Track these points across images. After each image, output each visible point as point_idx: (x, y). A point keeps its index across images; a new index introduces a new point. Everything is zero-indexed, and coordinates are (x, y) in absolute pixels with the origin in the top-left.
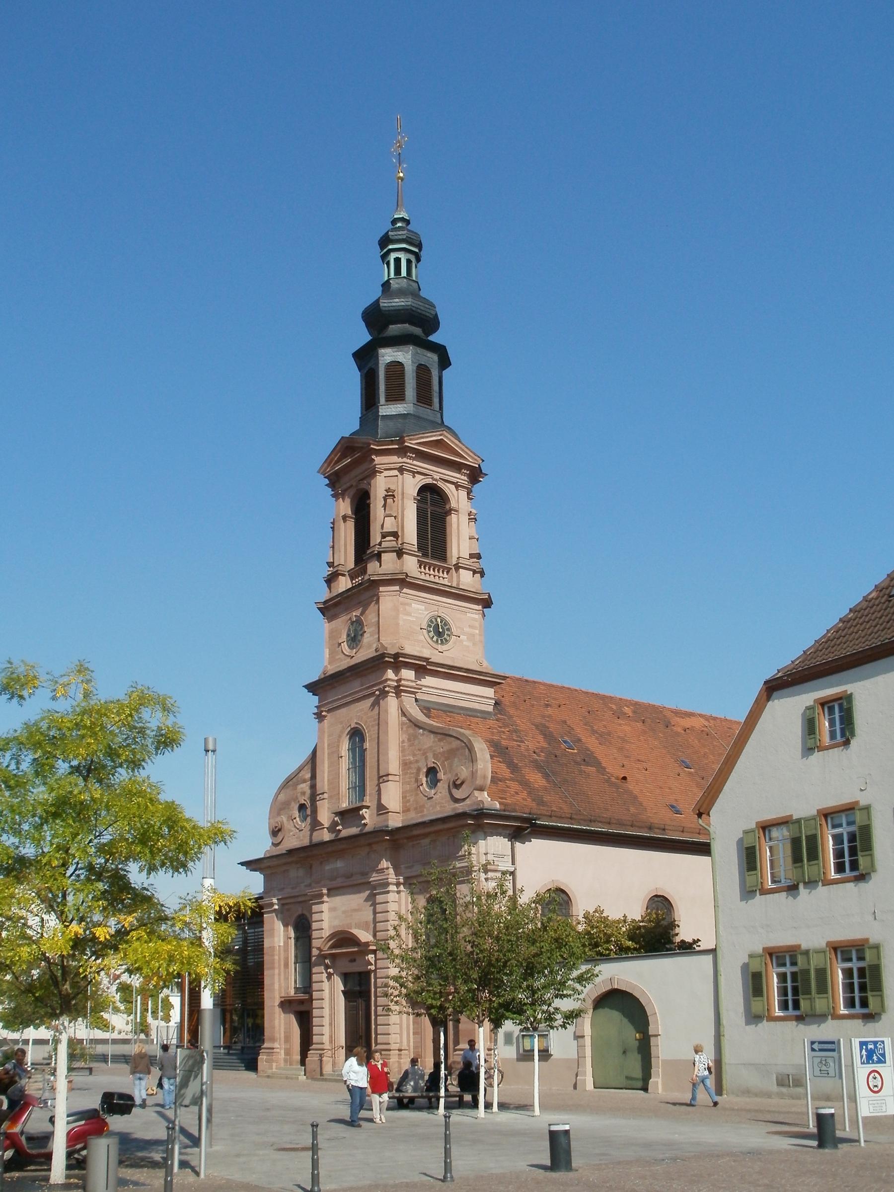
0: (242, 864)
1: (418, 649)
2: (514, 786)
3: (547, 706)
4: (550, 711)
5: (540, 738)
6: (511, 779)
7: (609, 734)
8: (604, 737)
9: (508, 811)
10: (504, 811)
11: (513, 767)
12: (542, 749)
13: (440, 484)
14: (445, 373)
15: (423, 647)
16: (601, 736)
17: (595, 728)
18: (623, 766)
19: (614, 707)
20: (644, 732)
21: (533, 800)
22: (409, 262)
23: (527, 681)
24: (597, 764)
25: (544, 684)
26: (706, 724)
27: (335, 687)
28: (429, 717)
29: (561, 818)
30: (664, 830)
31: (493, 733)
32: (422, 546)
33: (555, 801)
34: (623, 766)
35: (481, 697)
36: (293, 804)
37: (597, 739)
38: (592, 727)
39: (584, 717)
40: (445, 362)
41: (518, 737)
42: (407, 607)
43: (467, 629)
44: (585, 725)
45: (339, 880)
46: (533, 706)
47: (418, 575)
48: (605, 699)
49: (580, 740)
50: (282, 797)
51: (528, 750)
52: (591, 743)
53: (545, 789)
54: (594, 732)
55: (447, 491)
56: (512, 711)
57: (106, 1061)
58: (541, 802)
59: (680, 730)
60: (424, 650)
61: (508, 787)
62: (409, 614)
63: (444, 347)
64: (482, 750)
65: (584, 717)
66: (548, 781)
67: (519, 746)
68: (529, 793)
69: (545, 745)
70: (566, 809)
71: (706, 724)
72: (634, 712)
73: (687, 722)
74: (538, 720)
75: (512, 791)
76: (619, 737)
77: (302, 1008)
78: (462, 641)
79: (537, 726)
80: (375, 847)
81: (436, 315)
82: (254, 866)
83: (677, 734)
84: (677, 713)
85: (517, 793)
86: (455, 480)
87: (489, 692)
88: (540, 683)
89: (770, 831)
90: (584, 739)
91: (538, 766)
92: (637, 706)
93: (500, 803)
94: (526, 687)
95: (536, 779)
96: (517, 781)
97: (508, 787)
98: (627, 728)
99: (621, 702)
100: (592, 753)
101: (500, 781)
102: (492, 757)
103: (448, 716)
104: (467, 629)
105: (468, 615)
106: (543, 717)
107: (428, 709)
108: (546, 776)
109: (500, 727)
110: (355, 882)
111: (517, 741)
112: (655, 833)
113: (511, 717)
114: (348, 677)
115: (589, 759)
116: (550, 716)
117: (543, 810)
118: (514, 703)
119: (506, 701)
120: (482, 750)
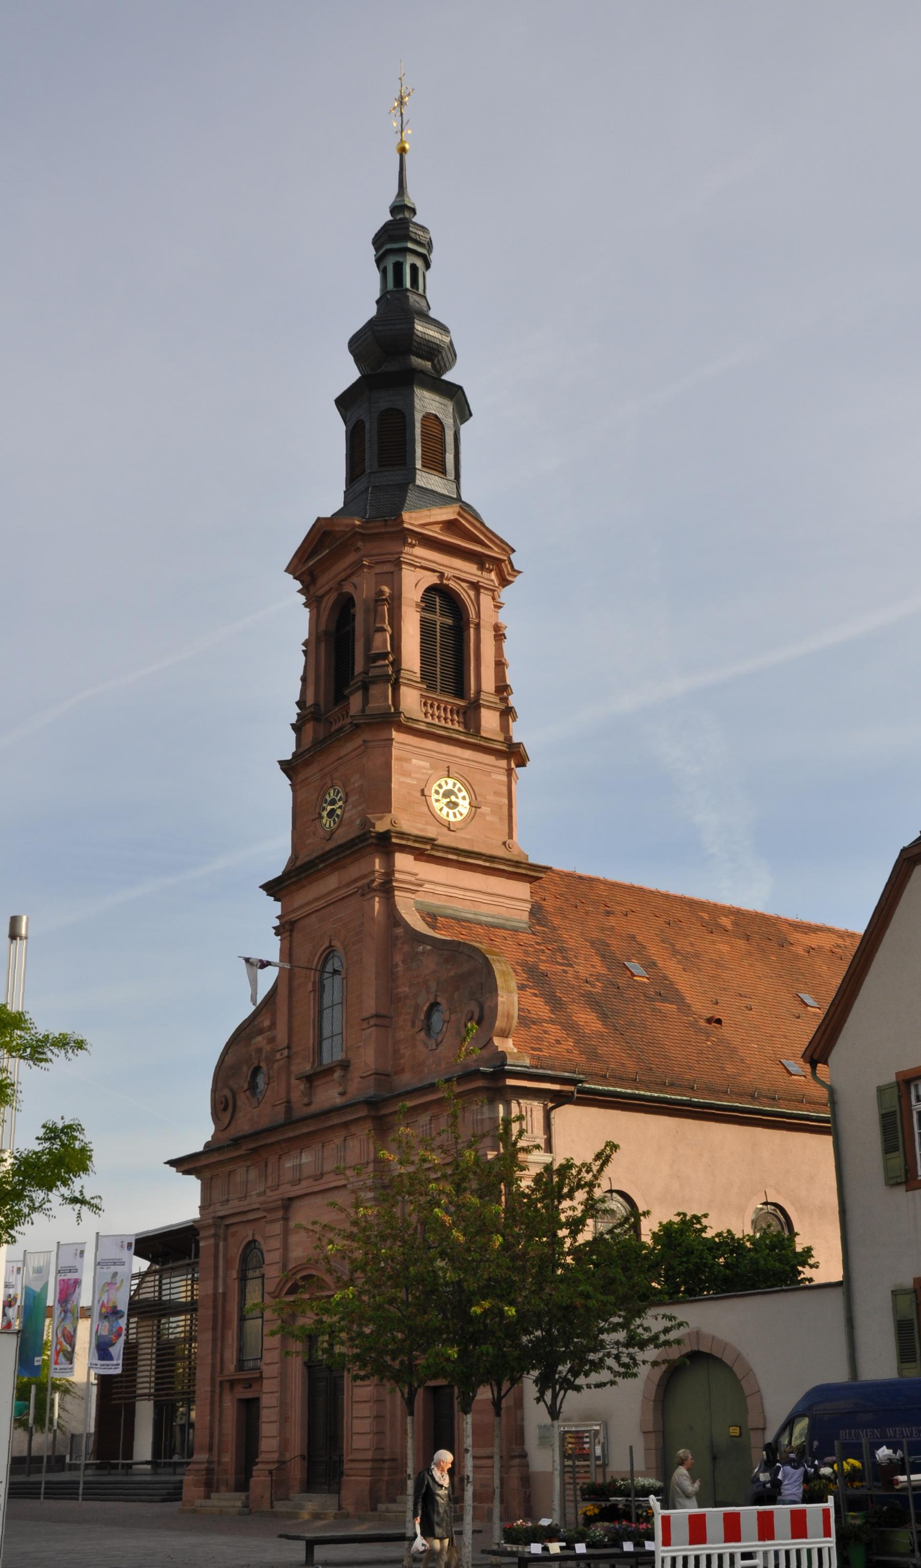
0: (172, 1163)
1: (420, 826)
2: (555, 1031)
3: (608, 913)
4: (612, 921)
5: (596, 960)
6: (552, 1022)
7: (697, 956)
8: (689, 960)
9: (541, 1068)
10: (536, 1067)
11: (555, 1003)
12: (598, 977)
13: (452, 584)
14: (464, 429)
15: (427, 823)
16: (686, 958)
17: (678, 947)
18: (717, 1003)
19: (706, 916)
20: (750, 954)
21: (582, 1053)
22: (414, 268)
23: (581, 878)
24: (678, 999)
25: (605, 882)
26: (840, 942)
27: (303, 887)
28: (433, 927)
29: (621, 1080)
30: (774, 1099)
31: (526, 953)
32: (427, 676)
33: (615, 1054)
34: (717, 1003)
35: (509, 900)
36: (245, 1069)
37: (679, 962)
38: (673, 945)
39: (662, 931)
40: (463, 412)
41: (564, 958)
42: (405, 764)
43: (490, 798)
44: (663, 941)
45: (304, 1184)
46: (587, 913)
47: (421, 717)
48: (693, 906)
49: (654, 964)
50: (230, 1059)
51: (577, 977)
52: (671, 968)
53: (601, 1035)
54: (675, 952)
55: (464, 596)
56: (557, 922)
57: (117, 1468)
58: (593, 1055)
59: (800, 951)
60: (429, 828)
61: (546, 1032)
62: (407, 774)
63: (460, 388)
64: (503, 973)
65: (662, 931)
66: (605, 1024)
67: (565, 972)
68: (577, 1042)
69: (603, 971)
70: (631, 1067)
71: (840, 942)
72: (735, 924)
73: (813, 940)
74: (596, 934)
75: (552, 1039)
76: (712, 960)
77: (249, 1395)
78: (483, 815)
79: (592, 943)
80: (354, 1129)
81: (451, 342)
82: (186, 1167)
83: (796, 957)
84: (798, 927)
85: (558, 1042)
86: (474, 579)
87: (522, 890)
88: (598, 880)
89: (916, 1086)
90: (660, 964)
91: (593, 1002)
92: (737, 914)
93: (533, 1057)
94: (579, 887)
95: (588, 1020)
96: (560, 1024)
97: (546, 1032)
98: (725, 948)
99: (715, 910)
100: (672, 983)
101: (534, 1023)
102: (522, 987)
103: (463, 927)
104: (490, 798)
105: (494, 776)
106: (603, 929)
107: (434, 917)
108: (603, 1017)
109: (538, 944)
110: (327, 1186)
111: (561, 964)
112: (761, 1104)
113: (555, 929)
114: (321, 870)
115: (666, 991)
116: (612, 928)
117: (596, 1067)
118: (561, 908)
119: (549, 905)
120: (503, 973)
